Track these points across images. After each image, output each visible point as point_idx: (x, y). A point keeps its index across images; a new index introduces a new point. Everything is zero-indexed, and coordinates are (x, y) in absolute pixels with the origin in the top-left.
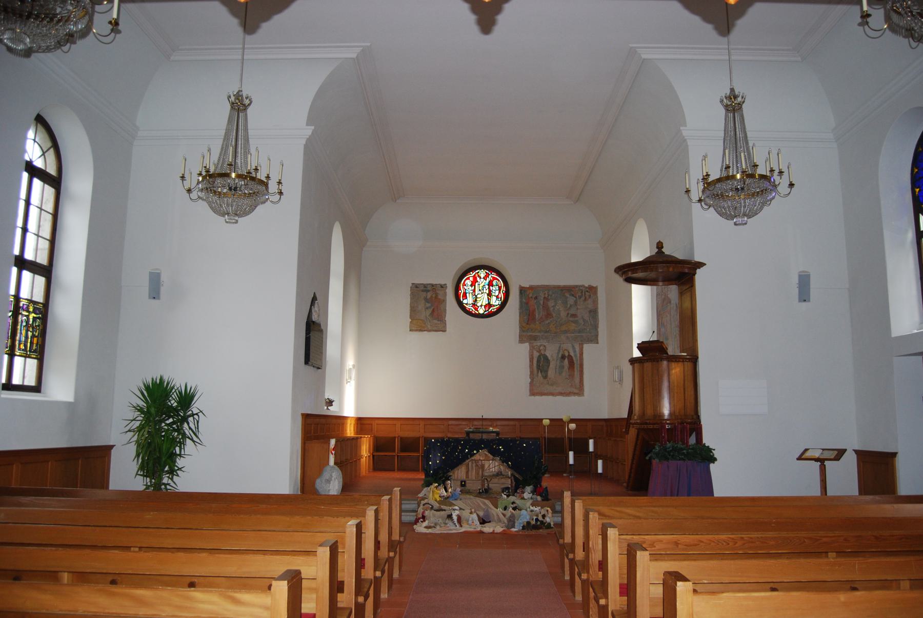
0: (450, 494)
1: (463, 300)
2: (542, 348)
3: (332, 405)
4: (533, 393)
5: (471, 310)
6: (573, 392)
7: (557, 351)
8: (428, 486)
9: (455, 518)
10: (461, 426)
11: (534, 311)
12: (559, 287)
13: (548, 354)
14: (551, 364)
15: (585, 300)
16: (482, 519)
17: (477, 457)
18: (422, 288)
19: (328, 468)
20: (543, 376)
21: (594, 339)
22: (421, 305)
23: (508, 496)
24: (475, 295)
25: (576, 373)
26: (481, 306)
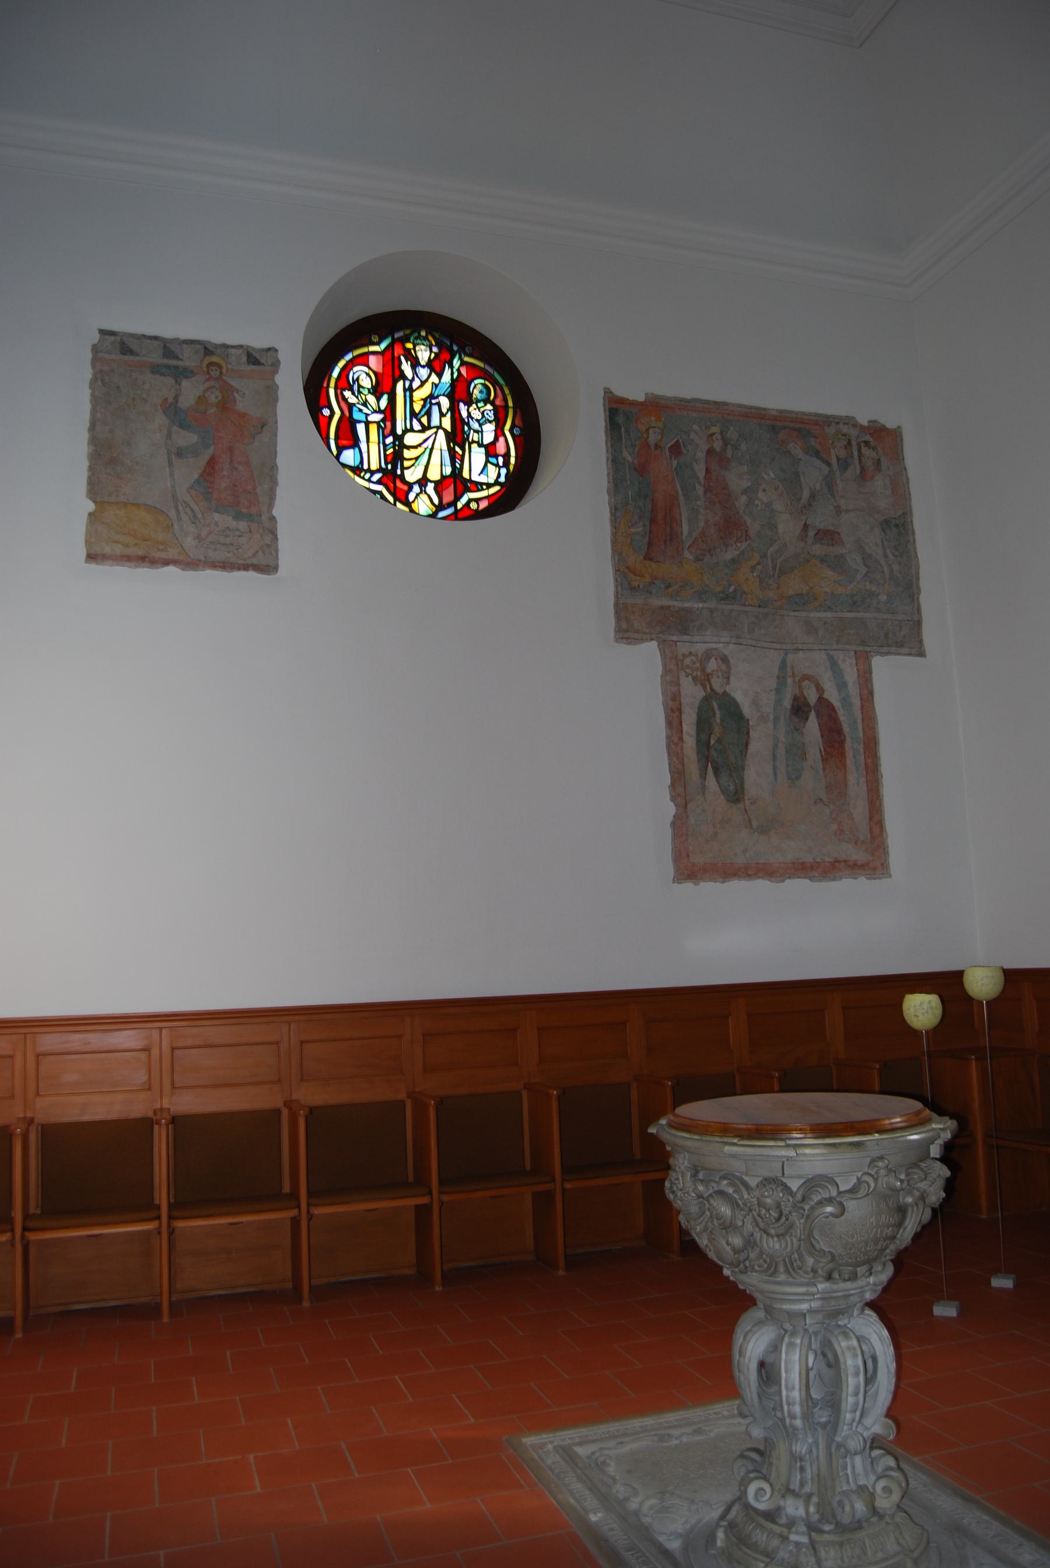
2: (712, 665)
7: (772, 683)
13: (740, 692)
14: (753, 734)
15: (863, 476)
18: (156, 357)
25: (852, 779)
26: (423, 482)
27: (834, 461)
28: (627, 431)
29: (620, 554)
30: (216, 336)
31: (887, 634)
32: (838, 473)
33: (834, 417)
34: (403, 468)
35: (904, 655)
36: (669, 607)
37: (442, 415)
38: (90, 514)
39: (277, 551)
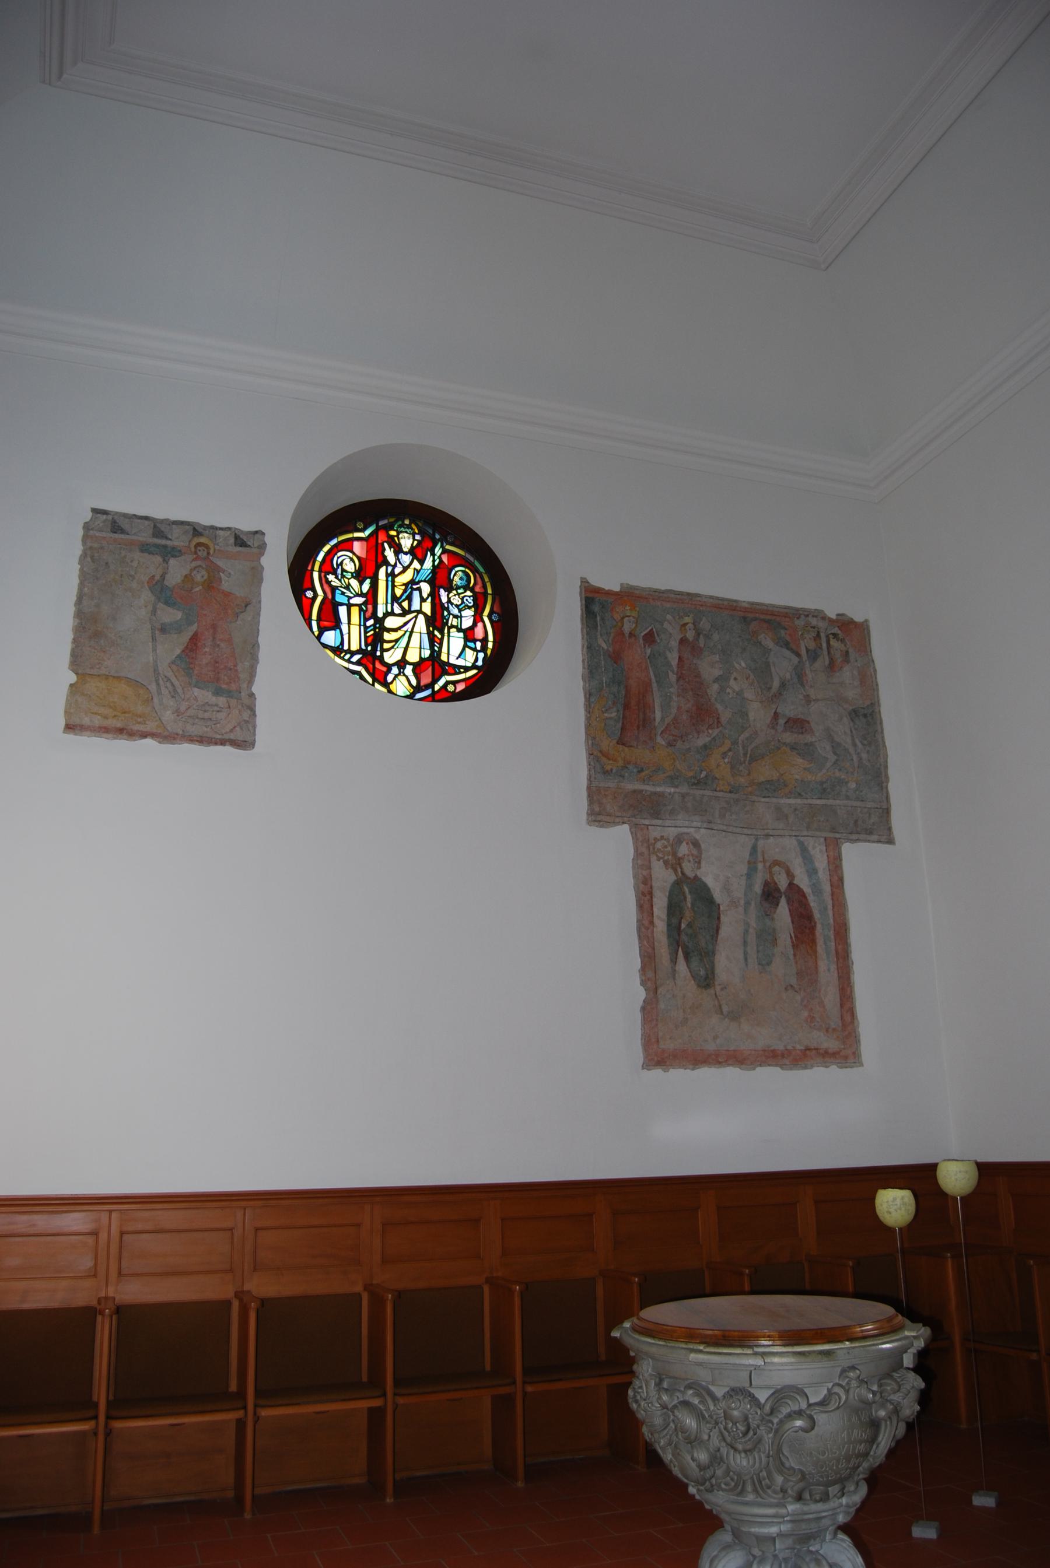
2: (684, 850)
7: (743, 869)
12: (730, 607)
13: (711, 877)
15: (832, 667)
18: (145, 536)
20: (694, 976)
26: (402, 663)
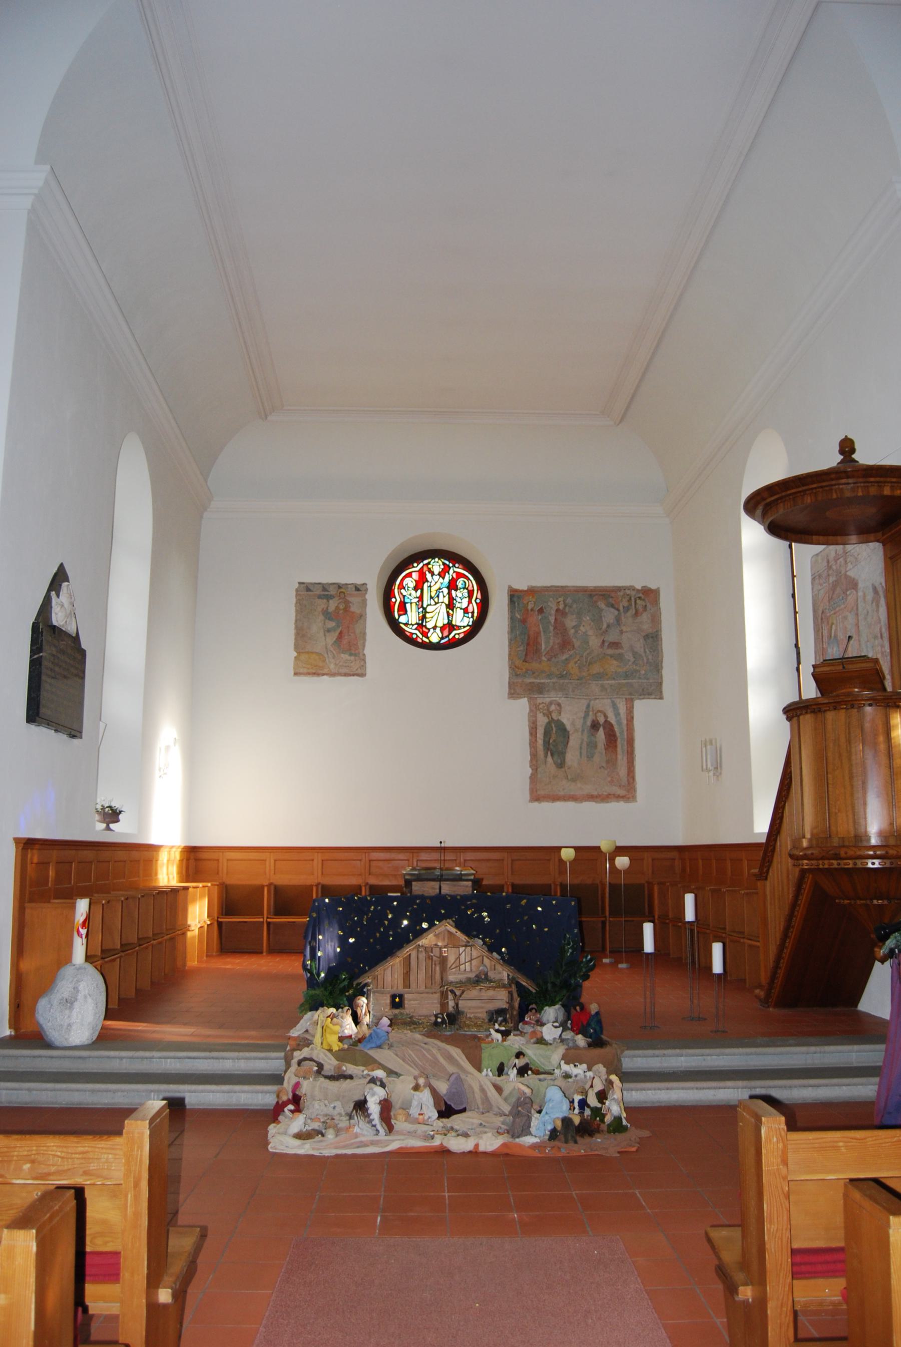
0: (365, 1028)
1: (399, 616)
2: (553, 707)
3: (118, 821)
4: (536, 797)
5: (414, 636)
6: (614, 795)
7: (582, 715)
8: (314, 1008)
9: (374, 1108)
10: (395, 863)
11: (538, 634)
12: (584, 590)
15: (637, 614)
16: (446, 1103)
17: (427, 940)
19: (67, 972)
21: (654, 691)
22: (317, 626)
23: (505, 1034)
24: (422, 606)
25: (619, 757)
26: (435, 628)
27: (621, 609)
28: (518, 604)
29: (512, 660)
30: (342, 580)
31: (643, 690)
32: (623, 614)
33: (623, 587)
34: (426, 622)
35: (652, 699)
36: (533, 683)
37: (444, 597)
38: (295, 657)
39: (366, 668)
